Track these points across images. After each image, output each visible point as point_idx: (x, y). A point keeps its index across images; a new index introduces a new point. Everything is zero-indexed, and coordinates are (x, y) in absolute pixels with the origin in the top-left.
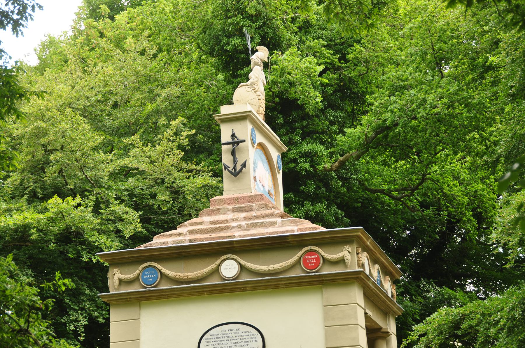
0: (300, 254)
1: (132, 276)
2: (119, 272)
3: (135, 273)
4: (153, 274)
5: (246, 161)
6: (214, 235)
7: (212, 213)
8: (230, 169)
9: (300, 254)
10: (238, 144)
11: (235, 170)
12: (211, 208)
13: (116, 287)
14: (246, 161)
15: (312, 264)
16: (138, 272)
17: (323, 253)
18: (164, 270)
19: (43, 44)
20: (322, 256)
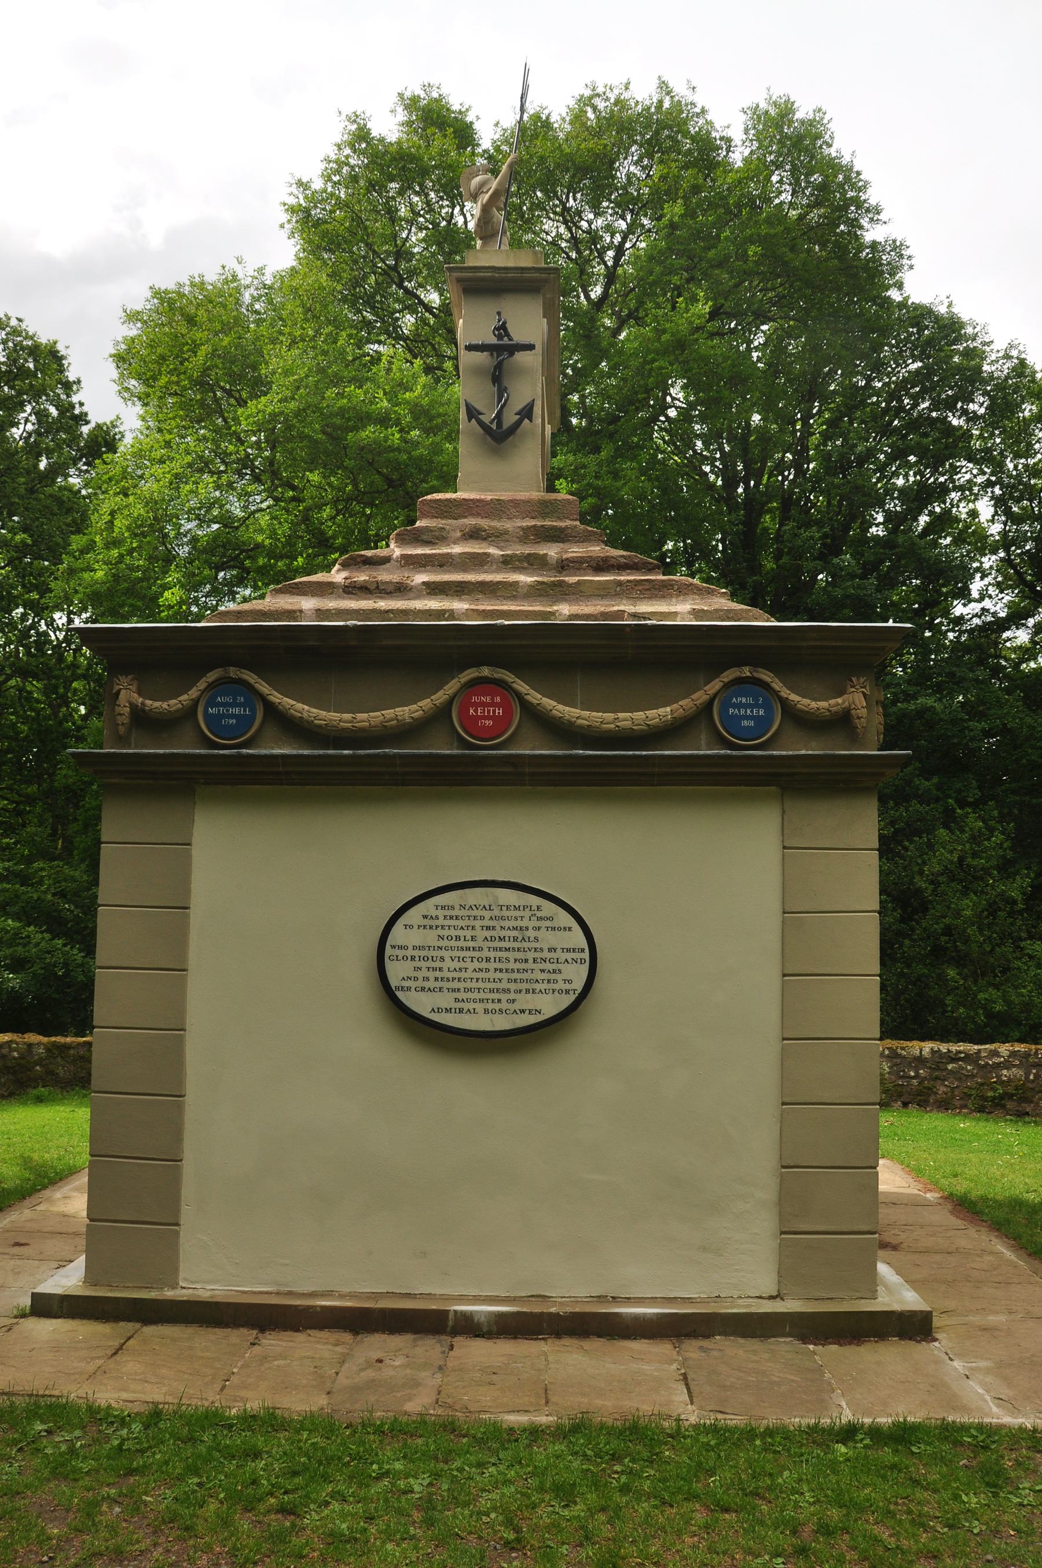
0: (715, 685)
1: (173, 704)
2: (134, 688)
3: (185, 697)
4: (240, 705)
5: (533, 400)
6: (382, 604)
7: (418, 538)
8: (485, 419)
9: (715, 685)
10: (512, 354)
11: (500, 424)
12: (418, 524)
13: (122, 730)
14: (533, 400)
15: (489, 723)
16: (194, 693)
17: (785, 693)
18: (276, 697)
19: (950, 328)
20: (780, 698)
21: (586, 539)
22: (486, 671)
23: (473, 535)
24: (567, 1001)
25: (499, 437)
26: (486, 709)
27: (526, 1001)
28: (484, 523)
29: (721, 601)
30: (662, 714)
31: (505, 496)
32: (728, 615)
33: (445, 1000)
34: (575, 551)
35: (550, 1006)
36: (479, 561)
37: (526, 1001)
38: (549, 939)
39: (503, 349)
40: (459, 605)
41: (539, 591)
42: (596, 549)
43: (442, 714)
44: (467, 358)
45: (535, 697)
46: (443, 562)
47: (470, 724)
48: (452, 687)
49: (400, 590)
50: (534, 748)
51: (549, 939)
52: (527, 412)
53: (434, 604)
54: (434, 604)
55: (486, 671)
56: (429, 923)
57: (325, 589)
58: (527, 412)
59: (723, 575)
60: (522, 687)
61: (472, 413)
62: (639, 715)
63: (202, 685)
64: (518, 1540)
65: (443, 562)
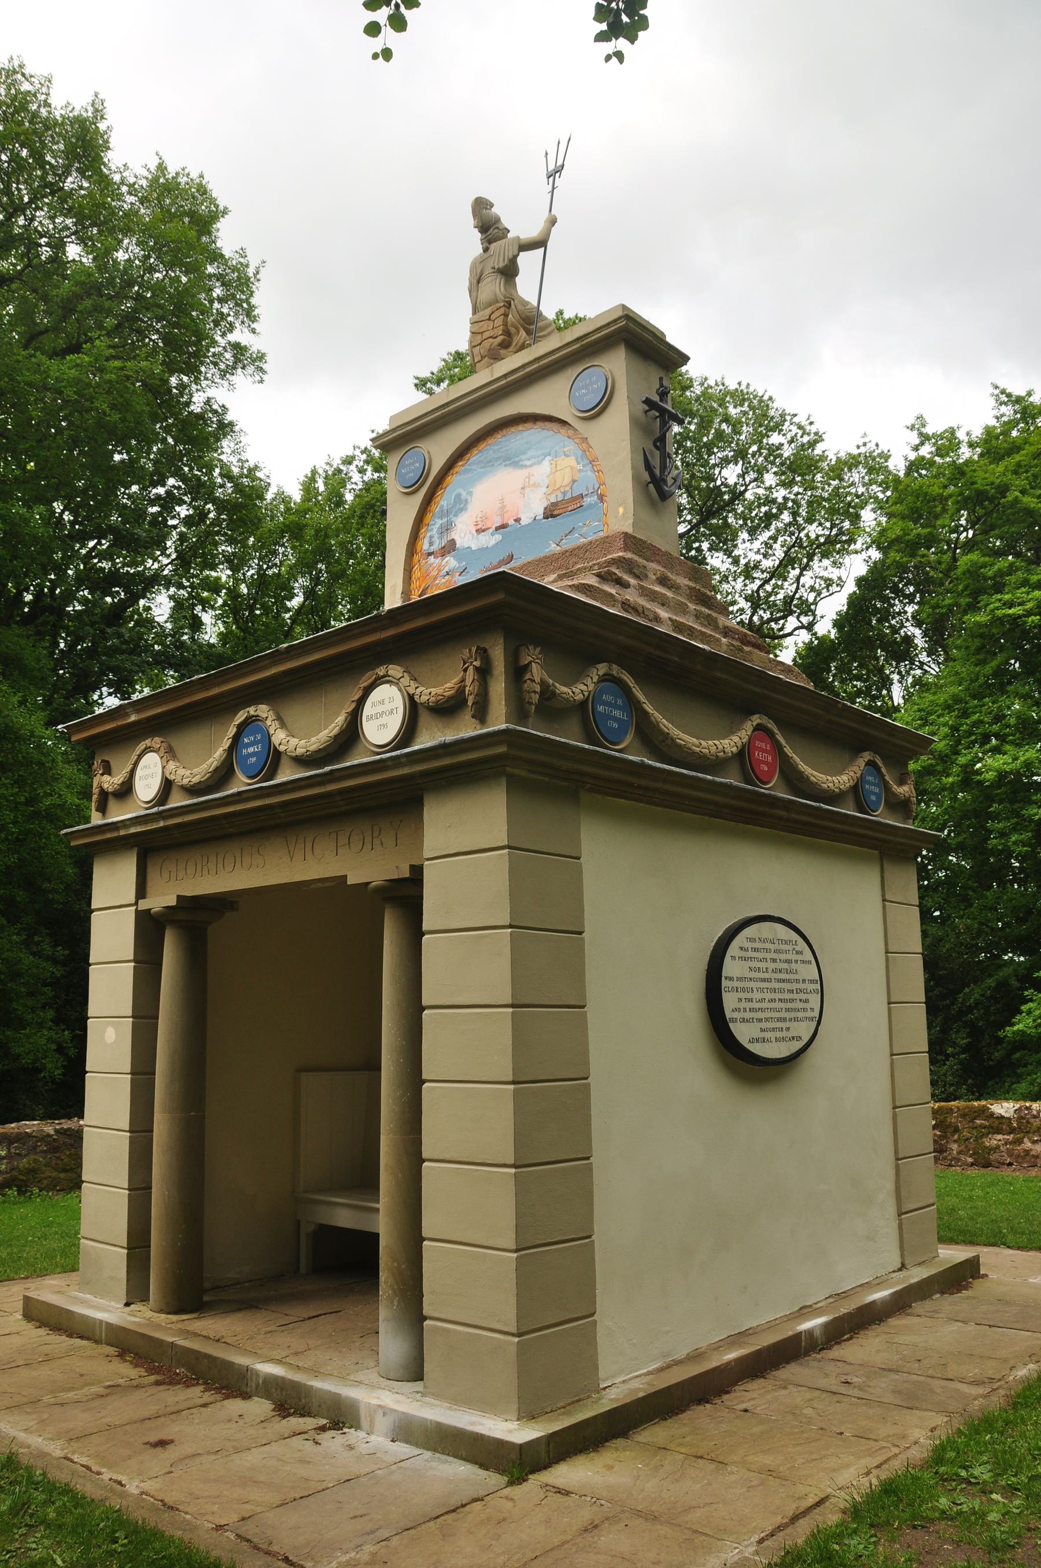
63: (232, 731)
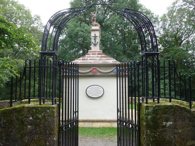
21: (103, 54)
22: (94, 67)
23: (93, 54)
24: (101, 95)
25: (95, 45)
26: (95, 71)
27: (98, 95)
28: (94, 53)
29: (115, 60)
30: (109, 71)
31: (96, 50)
32: (115, 62)
33: (92, 95)
34: (102, 55)
35: (100, 95)
36: (93, 57)
37: (98, 95)
38: (100, 90)
39: (95, 37)
40: (92, 61)
41: (99, 59)
42: (104, 55)
43: (91, 71)
44: (92, 38)
45: (99, 70)
46: (90, 57)
47: (93, 72)
48: (92, 69)
49: (87, 60)
50: (98, 74)
51: (100, 90)
52: (98, 43)
53: (90, 61)
54: (90, 61)
55: (94, 67)
56: (90, 89)
57: (80, 60)
58: (98, 43)
59: (9, 43)
60: (97, 69)
61: (93, 43)
62: (107, 71)
64: (84, 39)
65: (90, 57)
